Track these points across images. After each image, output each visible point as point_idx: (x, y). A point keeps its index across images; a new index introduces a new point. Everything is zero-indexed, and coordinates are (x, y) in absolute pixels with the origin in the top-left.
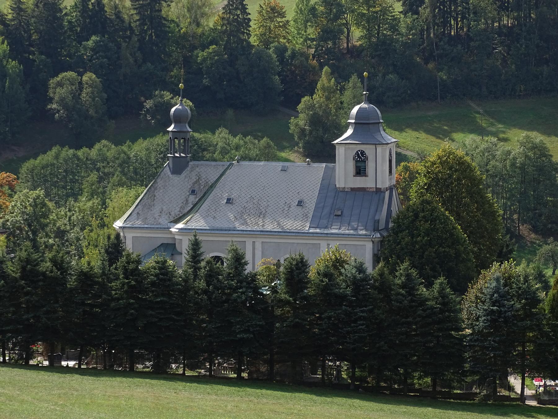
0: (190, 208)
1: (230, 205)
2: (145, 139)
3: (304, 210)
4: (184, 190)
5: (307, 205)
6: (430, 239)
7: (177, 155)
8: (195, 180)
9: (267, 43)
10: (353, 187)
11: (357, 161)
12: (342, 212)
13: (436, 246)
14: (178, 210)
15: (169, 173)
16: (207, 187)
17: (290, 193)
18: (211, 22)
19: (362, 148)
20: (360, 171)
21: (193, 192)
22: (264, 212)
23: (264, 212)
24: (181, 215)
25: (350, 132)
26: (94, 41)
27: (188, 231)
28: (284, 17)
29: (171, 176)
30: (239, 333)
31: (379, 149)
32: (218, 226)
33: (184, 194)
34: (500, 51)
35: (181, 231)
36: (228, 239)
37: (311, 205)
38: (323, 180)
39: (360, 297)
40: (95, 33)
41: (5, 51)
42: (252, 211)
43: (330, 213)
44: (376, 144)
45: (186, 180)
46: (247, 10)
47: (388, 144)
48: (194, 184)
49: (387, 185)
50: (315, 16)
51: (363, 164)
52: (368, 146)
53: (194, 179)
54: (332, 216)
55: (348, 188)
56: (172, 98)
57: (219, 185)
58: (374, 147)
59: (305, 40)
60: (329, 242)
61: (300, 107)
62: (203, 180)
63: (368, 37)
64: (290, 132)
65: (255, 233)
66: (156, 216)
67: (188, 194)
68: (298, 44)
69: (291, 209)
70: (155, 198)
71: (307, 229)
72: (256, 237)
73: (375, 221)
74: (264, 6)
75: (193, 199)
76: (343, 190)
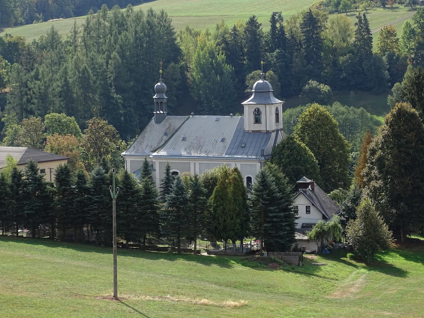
0: (163, 143)
1: (184, 141)
2: (290, 109)
3: (224, 144)
4: (161, 133)
5: (226, 141)
6: (290, 161)
7: (158, 112)
8: (168, 127)
10: (253, 130)
11: (255, 115)
12: (245, 145)
13: (293, 164)
14: (157, 144)
15: (154, 123)
16: (174, 131)
17: (219, 134)
18: (352, 40)
19: (258, 106)
20: (257, 121)
21: (166, 134)
22: (202, 145)
23: (202, 145)
24: (158, 147)
25: (253, 97)
26: (277, 52)
27: (159, 157)
29: (155, 124)
30: (27, 210)
31: (268, 107)
32: (175, 153)
33: (161, 135)
35: (154, 157)
36: (165, 161)
37: (228, 141)
38: (238, 126)
39: (98, 189)
40: (278, 48)
41: (223, 59)
42: (195, 145)
43: (239, 146)
44: (265, 104)
45: (163, 127)
46: (370, 32)
47: (273, 104)
48: (167, 129)
49: (274, 128)
50: (414, 35)
51: (259, 116)
52: (261, 106)
53: (167, 126)
54: (239, 147)
55: (251, 131)
56: (319, 85)
58: (264, 106)
59: (409, 50)
60: (236, 163)
61: (393, 89)
62: (172, 127)
64: (388, 104)
65: (204, 158)
66: (144, 148)
67: (163, 135)
68: (404, 52)
69: (217, 143)
70: (145, 138)
71: (224, 155)
72: (196, 160)
73: (262, 150)
74: (383, 30)
75: (165, 138)
76: (248, 132)
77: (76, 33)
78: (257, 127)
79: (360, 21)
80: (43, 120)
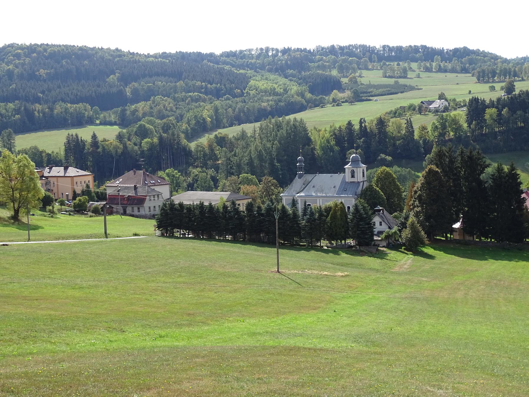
9: (420, 138)
18: (403, 132)
19: (353, 169)
20: (353, 176)
25: (350, 163)
28: (427, 130)
31: (358, 169)
34: (171, 127)
37: (337, 188)
49: (362, 180)
57: (312, 181)
59: (434, 137)
63: (455, 135)
66: (292, 192)
68: (432, 138)
75: (304, 186)
77: (255, 131)
78: (353, 180)
79: (408, 122)
80: (239, 178)
